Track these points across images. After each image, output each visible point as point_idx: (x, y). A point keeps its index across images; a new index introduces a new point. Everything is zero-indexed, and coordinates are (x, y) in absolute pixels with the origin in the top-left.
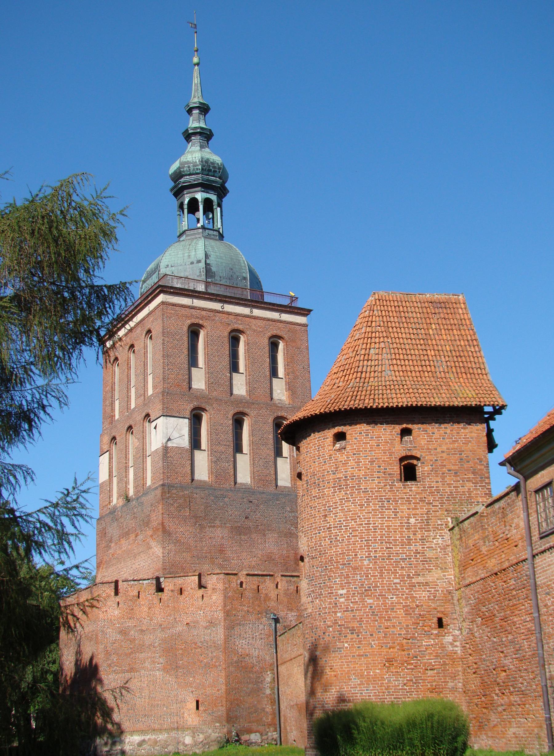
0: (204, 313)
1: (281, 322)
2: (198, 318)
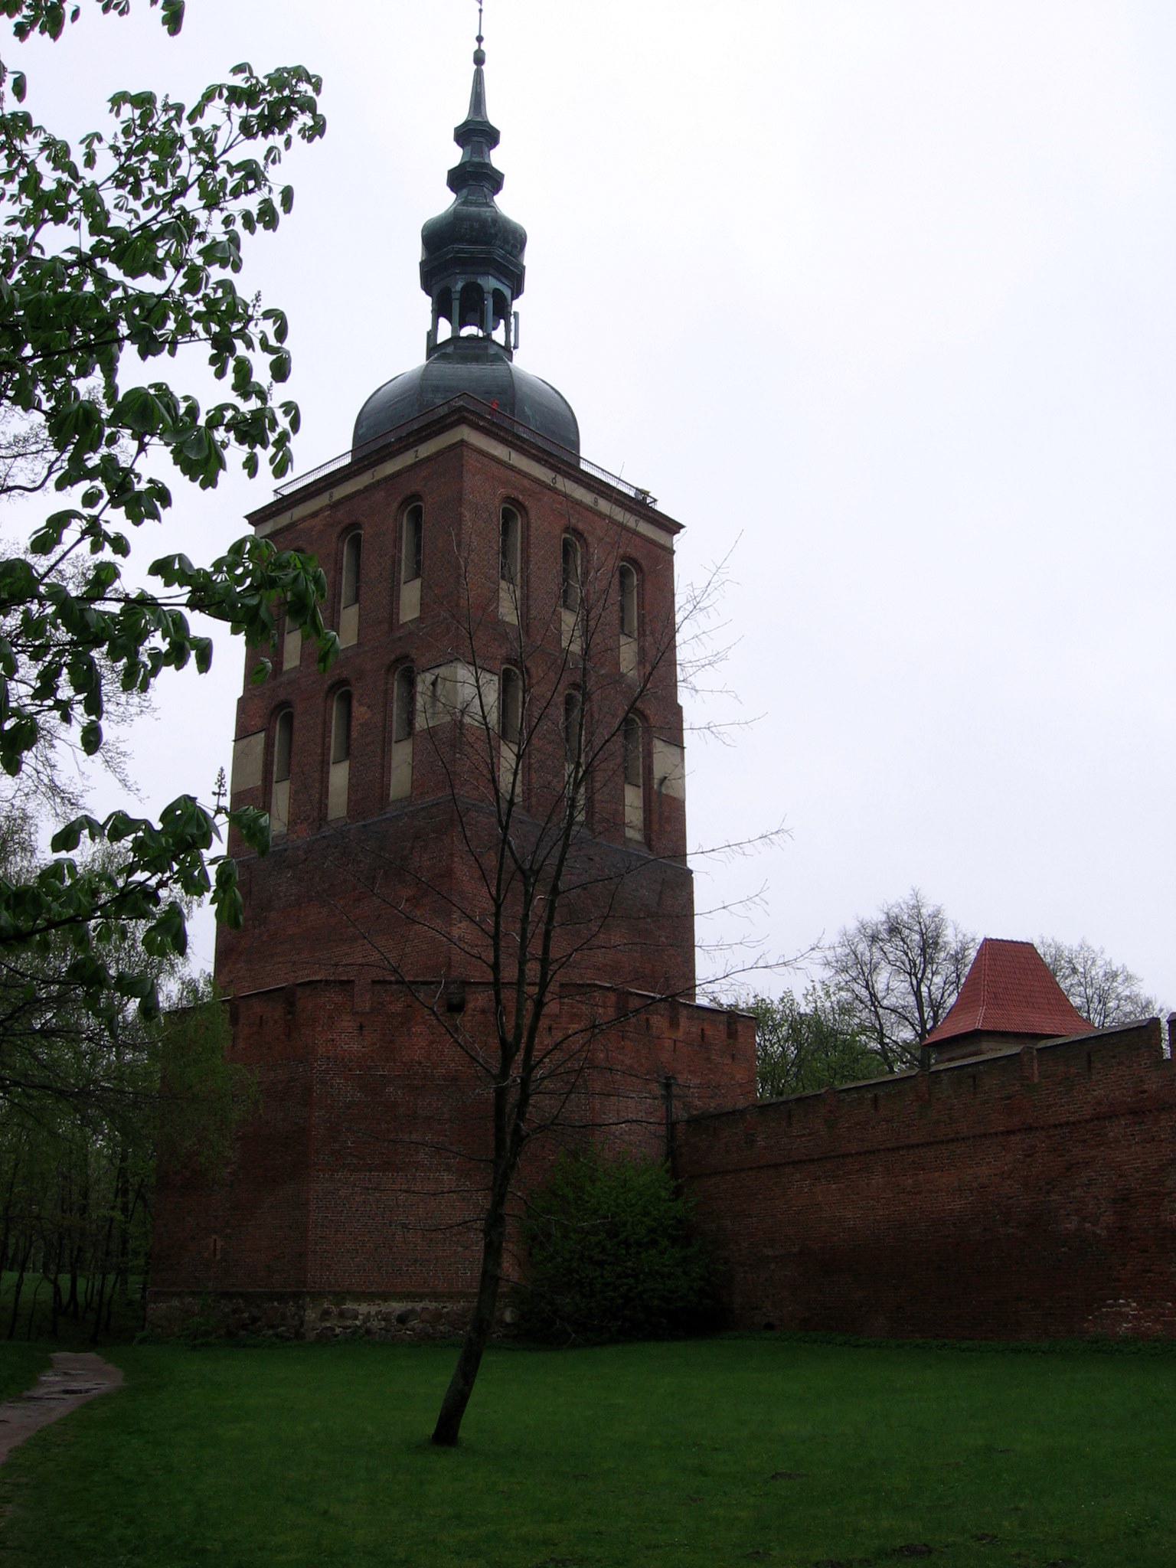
0: (526, 482)
1: (635, 533)
2: (516, 488)
